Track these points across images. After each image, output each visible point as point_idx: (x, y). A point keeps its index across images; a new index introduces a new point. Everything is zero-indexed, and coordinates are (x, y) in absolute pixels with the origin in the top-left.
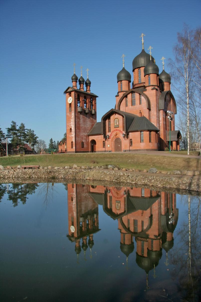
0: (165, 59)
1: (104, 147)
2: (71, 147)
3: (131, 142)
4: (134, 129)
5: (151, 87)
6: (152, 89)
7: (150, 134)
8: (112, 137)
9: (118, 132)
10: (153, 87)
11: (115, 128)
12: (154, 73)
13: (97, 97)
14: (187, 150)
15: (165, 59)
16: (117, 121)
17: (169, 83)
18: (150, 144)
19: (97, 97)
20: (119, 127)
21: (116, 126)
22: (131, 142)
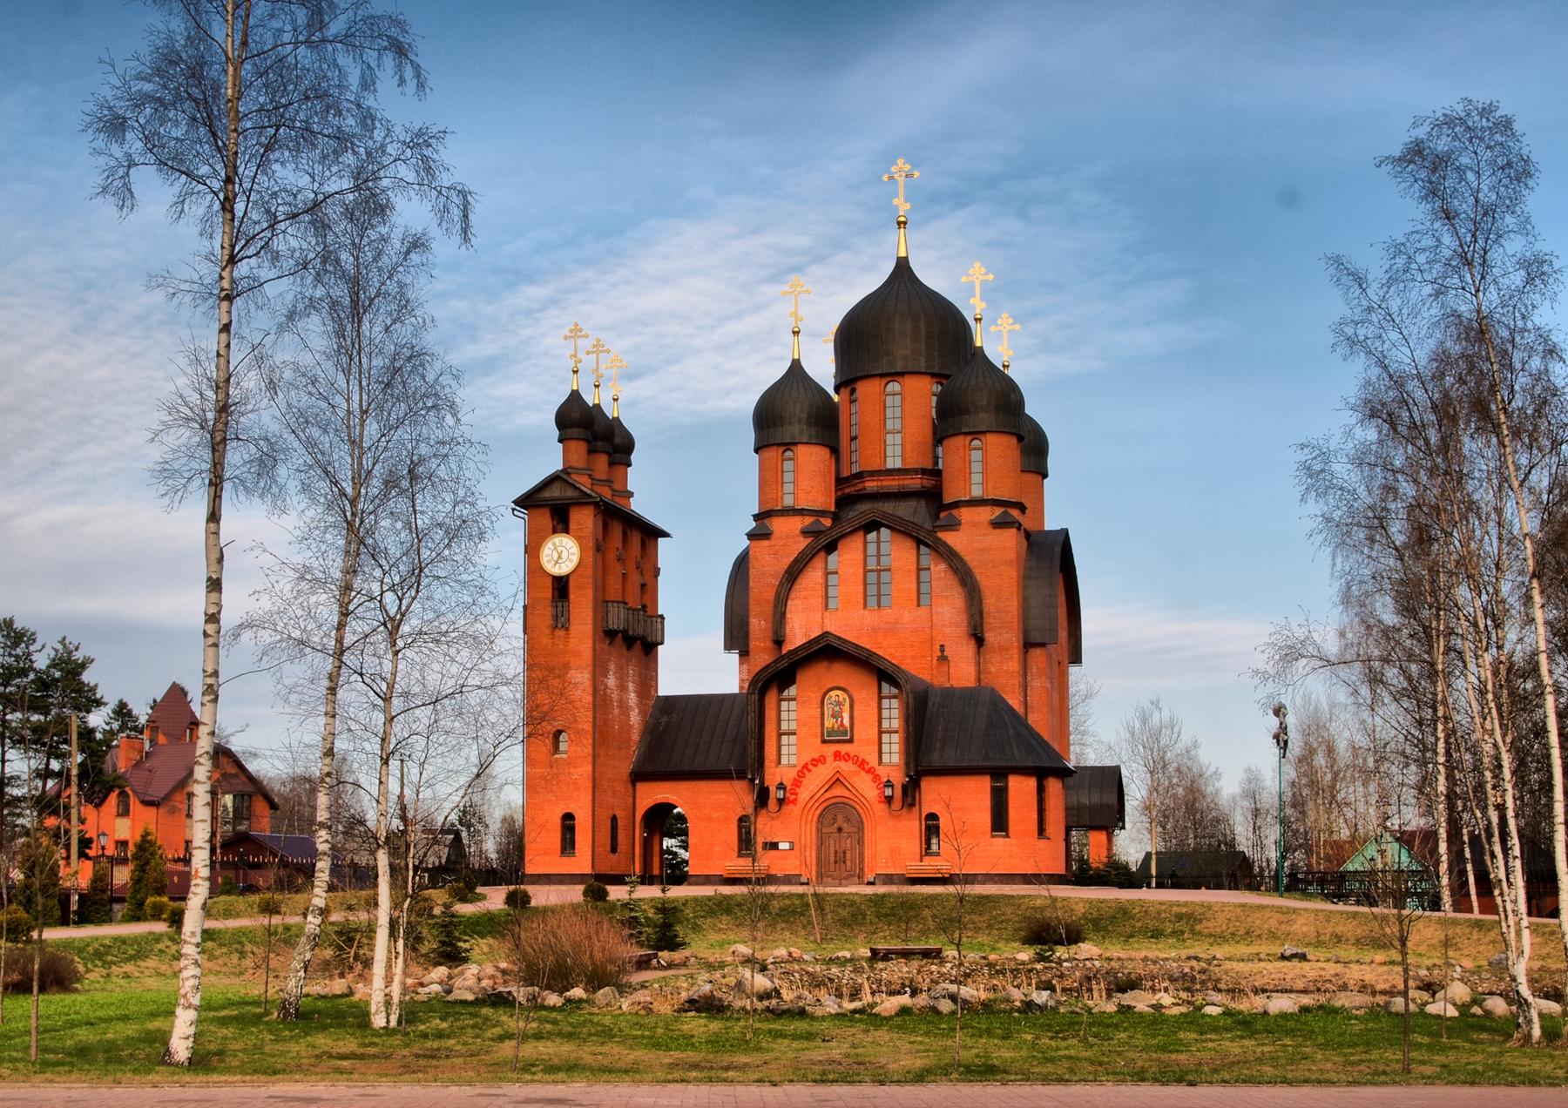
0: (991, 277)
1: (747, 856)
2: (559, 845)
3: (932, 827)
4: (951, 758)
5: (989, 509)
6: (997, 524)
7: (1041, 790)
8: (804, 794)
9: (846, 767)
10: (999, 511)
11: (824, 741)
12: (936, 370)
13: (665, 535)
14: (376, 886)
15: (991, 277)
16: (839, 704)
17: (1014, 441)
18: (1043, 844)
19: (665, 535)
20: (851, 741)
21: (832, 732)
22: (932, 827)
